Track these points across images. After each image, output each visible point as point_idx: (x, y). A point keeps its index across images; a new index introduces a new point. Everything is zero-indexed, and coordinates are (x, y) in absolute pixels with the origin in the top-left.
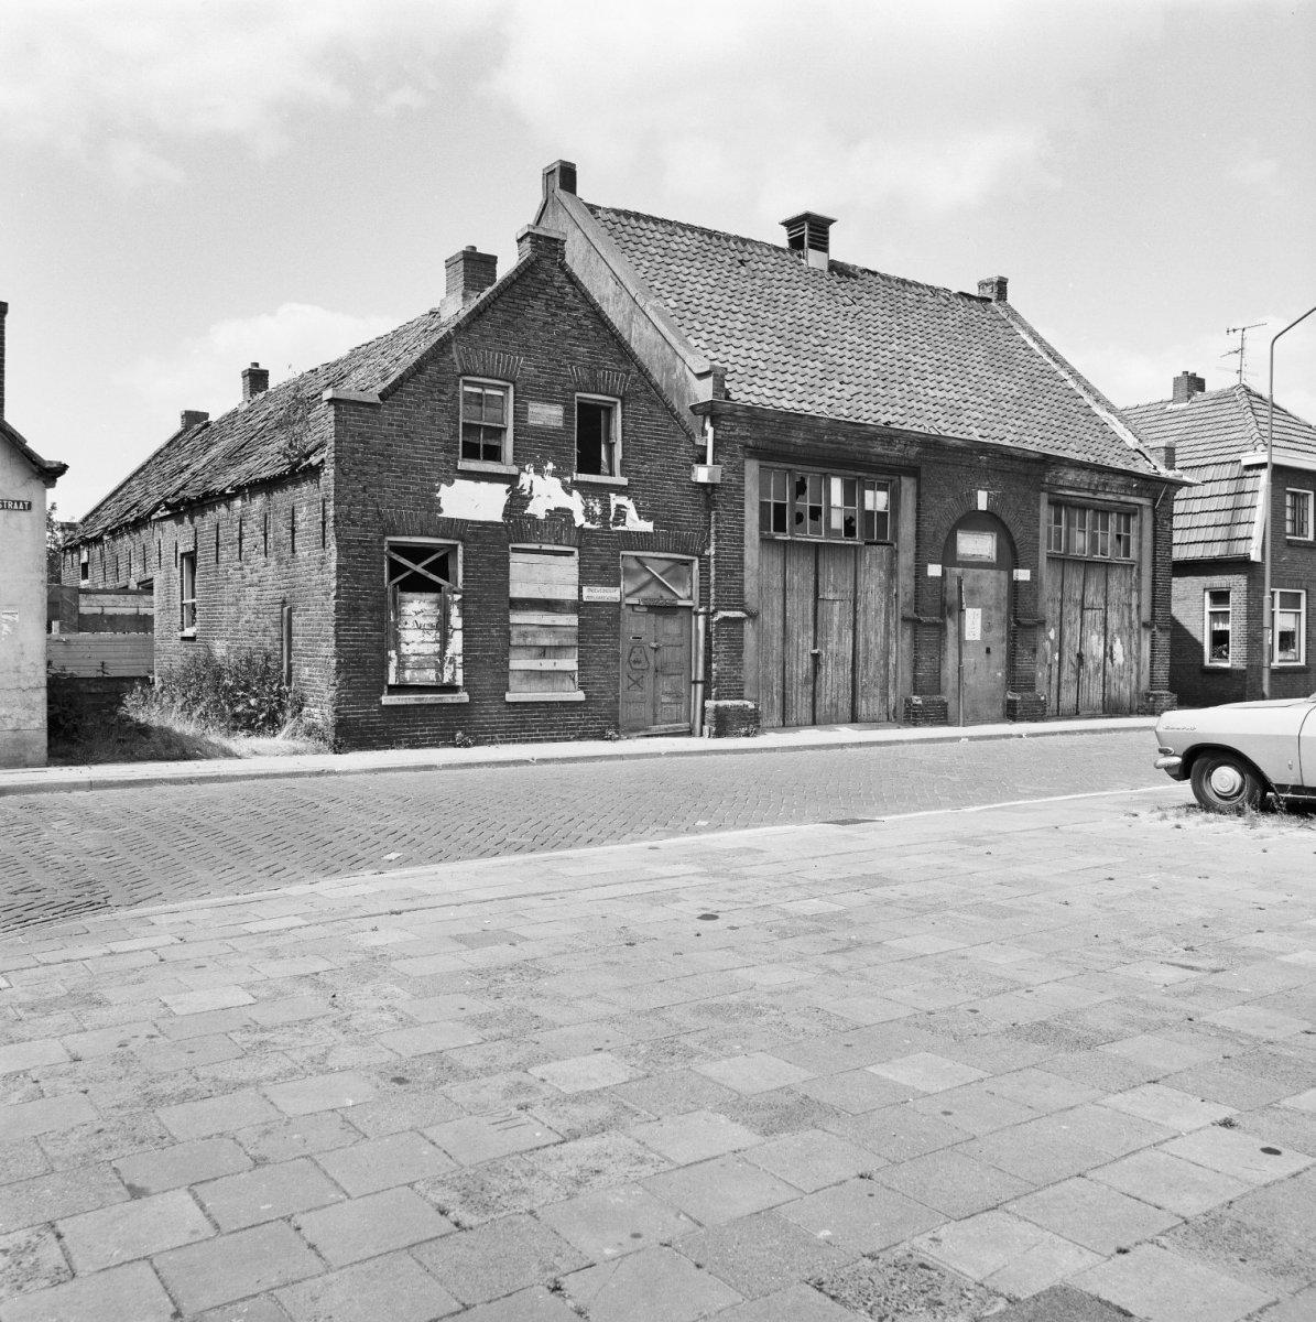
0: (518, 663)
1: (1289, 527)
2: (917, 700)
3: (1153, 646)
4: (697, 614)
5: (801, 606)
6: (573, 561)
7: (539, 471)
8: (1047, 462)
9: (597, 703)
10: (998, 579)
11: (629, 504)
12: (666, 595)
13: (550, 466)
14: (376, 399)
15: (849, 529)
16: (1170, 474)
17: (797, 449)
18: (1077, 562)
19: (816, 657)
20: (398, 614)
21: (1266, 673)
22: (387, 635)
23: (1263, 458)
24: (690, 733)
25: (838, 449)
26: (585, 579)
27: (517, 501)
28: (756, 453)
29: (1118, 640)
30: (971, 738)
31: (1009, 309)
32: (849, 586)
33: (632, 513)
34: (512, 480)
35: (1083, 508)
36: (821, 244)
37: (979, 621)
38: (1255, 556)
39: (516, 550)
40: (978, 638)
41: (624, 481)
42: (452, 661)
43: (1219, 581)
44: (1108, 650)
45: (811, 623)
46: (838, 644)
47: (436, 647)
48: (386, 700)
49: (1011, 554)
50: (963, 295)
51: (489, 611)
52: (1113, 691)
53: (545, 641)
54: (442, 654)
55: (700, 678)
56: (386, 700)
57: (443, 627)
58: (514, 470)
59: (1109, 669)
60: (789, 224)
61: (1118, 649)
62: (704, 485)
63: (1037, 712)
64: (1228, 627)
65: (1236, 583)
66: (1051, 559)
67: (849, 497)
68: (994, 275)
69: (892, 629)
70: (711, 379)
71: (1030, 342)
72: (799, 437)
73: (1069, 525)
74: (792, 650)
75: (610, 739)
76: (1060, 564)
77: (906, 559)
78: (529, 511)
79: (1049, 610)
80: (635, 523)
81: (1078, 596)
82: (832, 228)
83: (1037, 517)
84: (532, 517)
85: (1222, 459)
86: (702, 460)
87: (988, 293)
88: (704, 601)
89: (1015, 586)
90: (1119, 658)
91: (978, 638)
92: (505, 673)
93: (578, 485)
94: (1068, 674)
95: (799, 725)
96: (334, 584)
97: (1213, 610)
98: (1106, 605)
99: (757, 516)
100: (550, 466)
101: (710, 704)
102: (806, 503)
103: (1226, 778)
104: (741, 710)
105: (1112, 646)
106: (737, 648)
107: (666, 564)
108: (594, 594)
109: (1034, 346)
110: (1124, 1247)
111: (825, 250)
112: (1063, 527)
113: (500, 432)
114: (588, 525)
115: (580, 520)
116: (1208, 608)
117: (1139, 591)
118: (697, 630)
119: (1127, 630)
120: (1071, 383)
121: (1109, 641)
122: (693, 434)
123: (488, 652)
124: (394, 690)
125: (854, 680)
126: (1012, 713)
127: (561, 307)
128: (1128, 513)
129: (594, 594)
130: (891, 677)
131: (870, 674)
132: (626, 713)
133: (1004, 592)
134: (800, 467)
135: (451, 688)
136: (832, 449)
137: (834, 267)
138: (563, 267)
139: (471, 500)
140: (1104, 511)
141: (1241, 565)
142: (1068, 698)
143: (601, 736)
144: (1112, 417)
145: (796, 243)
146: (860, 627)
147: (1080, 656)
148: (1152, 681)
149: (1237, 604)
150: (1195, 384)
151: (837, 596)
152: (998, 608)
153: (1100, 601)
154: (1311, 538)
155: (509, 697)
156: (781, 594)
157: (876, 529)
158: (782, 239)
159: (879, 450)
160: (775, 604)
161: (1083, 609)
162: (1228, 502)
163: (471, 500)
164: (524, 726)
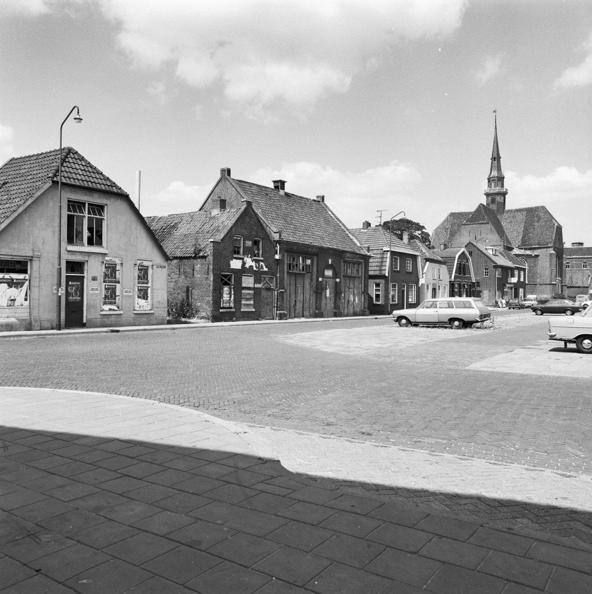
0: (243, 302)
1: (394, 266)
2: (317, 311)
3: (364, 298)
4: (275, 290)
5: (293, 288)
7: (247, 257)
8: (344, 252)
11: (263, 264)
12: (269, 286)
13: (249, 256)
14: (220, 241)
16: (368, 254)
17: (293, 250)
19: (295, 301)
20: (223, 291)
21: (389, 305)
22: (221, 296)
23: (388, 249)
24: (273, 319)
26: (255, 282)
27: (244, 264)
28: (287, 251)
30: (332, 320)
31: (325, 204)
32: (302, 283)
33: (264, 267)
34: (243, 259)
35: (350, 263)
36: (283, 188)
38: (387, 275)
39: (244, 276)
41: (262, 259)
43: (377, 281)
46: (300, 298)
47: (229, 298)
48: (221, 310)
49: (335, 275)
50: (314, 200)
51: (238, 289)
53: (248, 297)
54: (230, 300)
55: (276, 306)
56: (221, 310)
57: (230, 294)
58: (243, 257)
60: (274, 182)
61: (356, 299)
62: (277, 259)
63: (341, 315)
64: (380, 293)
65: (382, 282)
66: (343, 276)
67: (303, 262)
68: (321, 195)
69: (311, 294)
70: (278, 234)
71: (331, 215)
72: (295, 248)
73: (347, 267)
75: (260, 320)
77: (315, 277)
79: (343, 289)
80: (265, 269)
82: (286, 184)
83: (341, 265)
84: (246, 268)
85: (378, 248)
86: (276, 253)
87: (319, 199)
88: (276, 288)
89: (336, 283)
90: (357, 302)
92: (241, 304)
93: (254, 260)
94: (346, 306)
96: (212, 284)
97: (440, 297)
100: (249, 256)
101: (278, 312)
103: (404, 321)
104: (284, 313)
105: (355, 299)
106: (283, 298)
108: (257, 286)
109: (333, 216)
111: (284, 190)
112: (345, 267)
113: (239, 248)
114: (256, 269)
115: (255, 269)
116: (374, 288)
117: (361, 284)
118: (275, 295)
119: (358, 294)
120: (343, 228)
123: (238, 301)
125: (303, 307)
126: (335, 315)
128: (359, 264)
129: (257, 286)
130: (311, 306)
131: (306, 305)
132: (263, 314)
135: (231, 308)
137: (286, 194)
138: (252, 208)
139: (236, 264)
140: (354, 263)
141: (383, 277)
142: (346, 311)
143: (258, 320)
144: (353, 237)
145: (276, 187)
147: (348, 301)
148: (364, 307)
149: (382, 287)
150: (368, 224)
152: (333, 289)
154: (399, 270)
155: (242, 310)
157: (307, 268)
158: (272, 186)
159: (310, 250)
161: (349, 289)
162: (380, 260)
163: (236, 264)
164: (244, 317)
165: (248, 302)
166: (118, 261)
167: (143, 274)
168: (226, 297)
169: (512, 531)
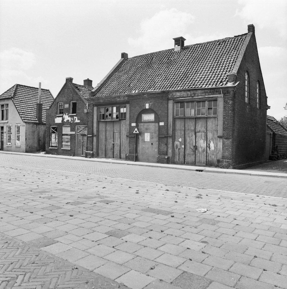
6: (70, 128)
9: (72, 150)
10: (155, 126)
12: (84, 133)
13: (67, 114)
15: (117, 117)
18: (190, 118)
20: (51, 136)
25: (109, 102)
27: (63, 119)
29: (212, 142)
33: (77, 119)
34: (62, 116)
37: (149, 137)
40: (149, 140)
42: (56, 143)
44: (208, 145)
45: (112, 137)
51: (61, 135)
52: (210, 158)
59: (208, 151)
61: (212, 145)
74: (107, 143)
76: (205, 120)
78: (64, 121)
80: (77, 121)
81: (193, 128)
84: (65, 122)
91: (149, 140)
95: (109, 158)
98: (207, 131)
99: (96, 117)
102: (108, 113)
107: (84, 127)
110: (72, 215)
115: (70, 121)
121: (208, 142)
122: (128, 96)
123: (60, 142)
124: (52, 146)
127: (69, 89)
133: (157, 129)
134: (107, 106)
136: (109, 102)
139: (58, 120)
146: (121, 139)
151: (117, 131)
152: (155, 133)
153: (203, 129)
156: (105, 131)
159: (118, 100)
160: (103, 133)
164: (64, 153)
165: (67, 144)
166: (11, 125)
167: (19, 128)
168: (53, 140)
169: (190, 227)
